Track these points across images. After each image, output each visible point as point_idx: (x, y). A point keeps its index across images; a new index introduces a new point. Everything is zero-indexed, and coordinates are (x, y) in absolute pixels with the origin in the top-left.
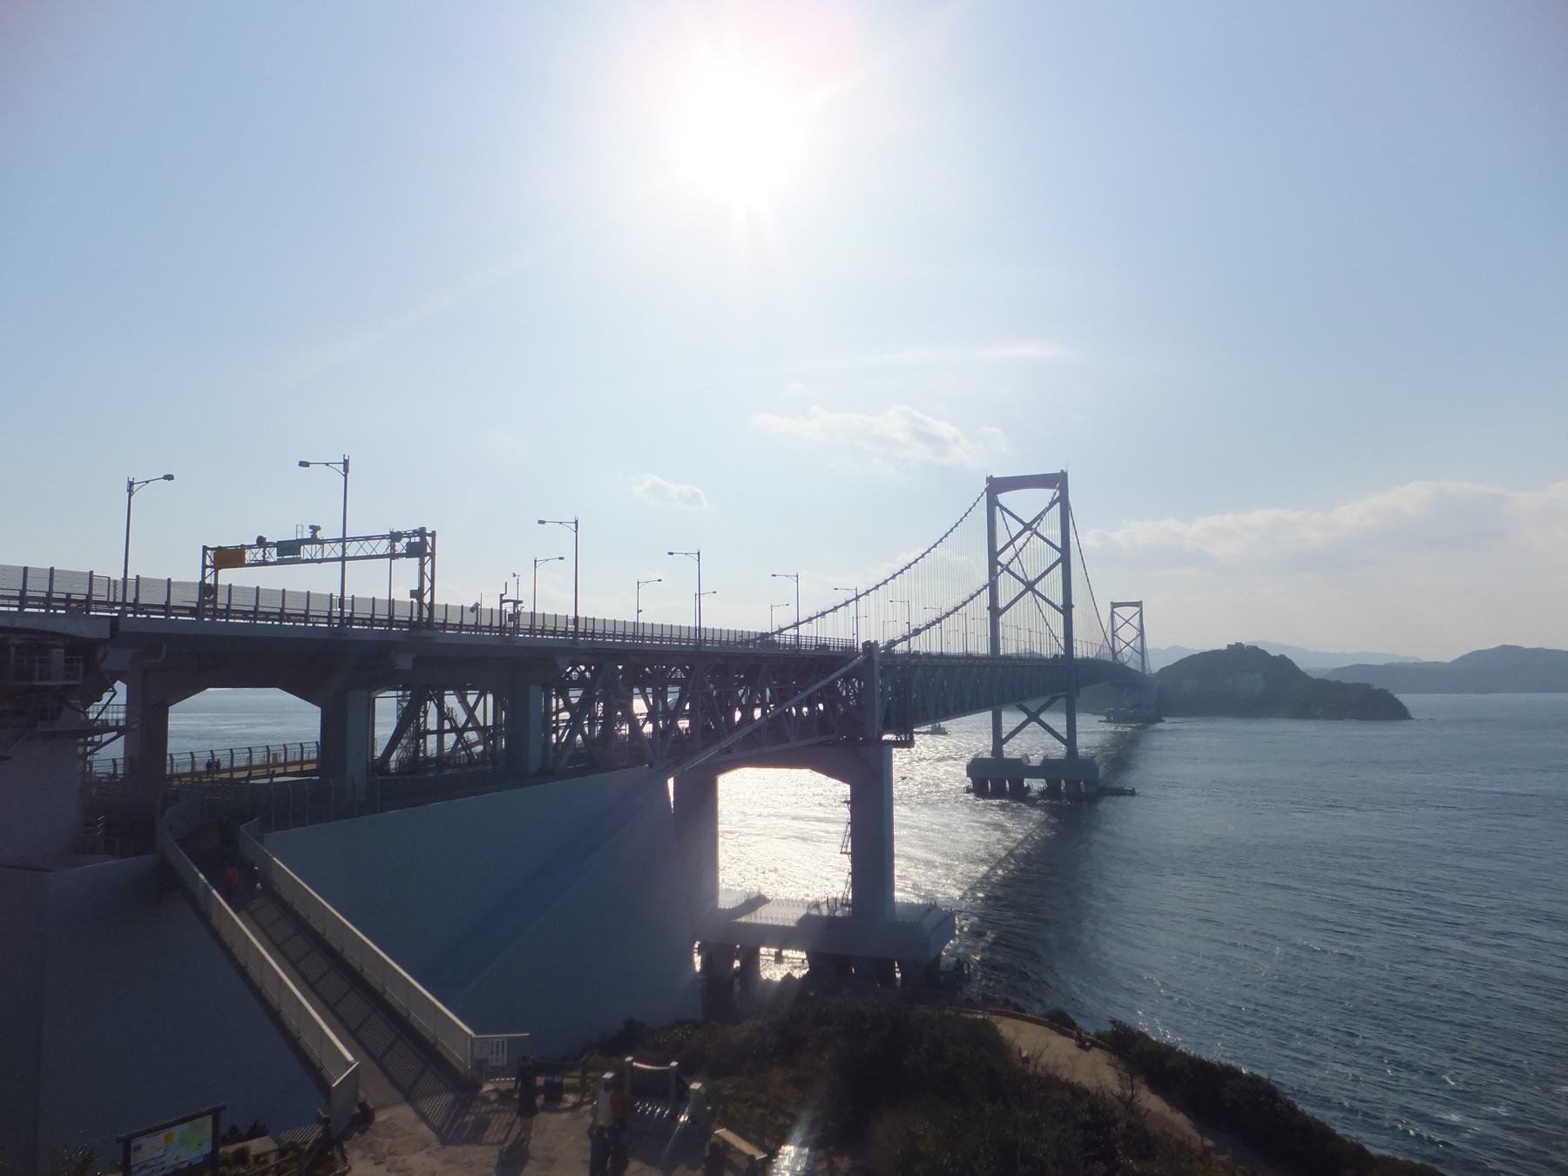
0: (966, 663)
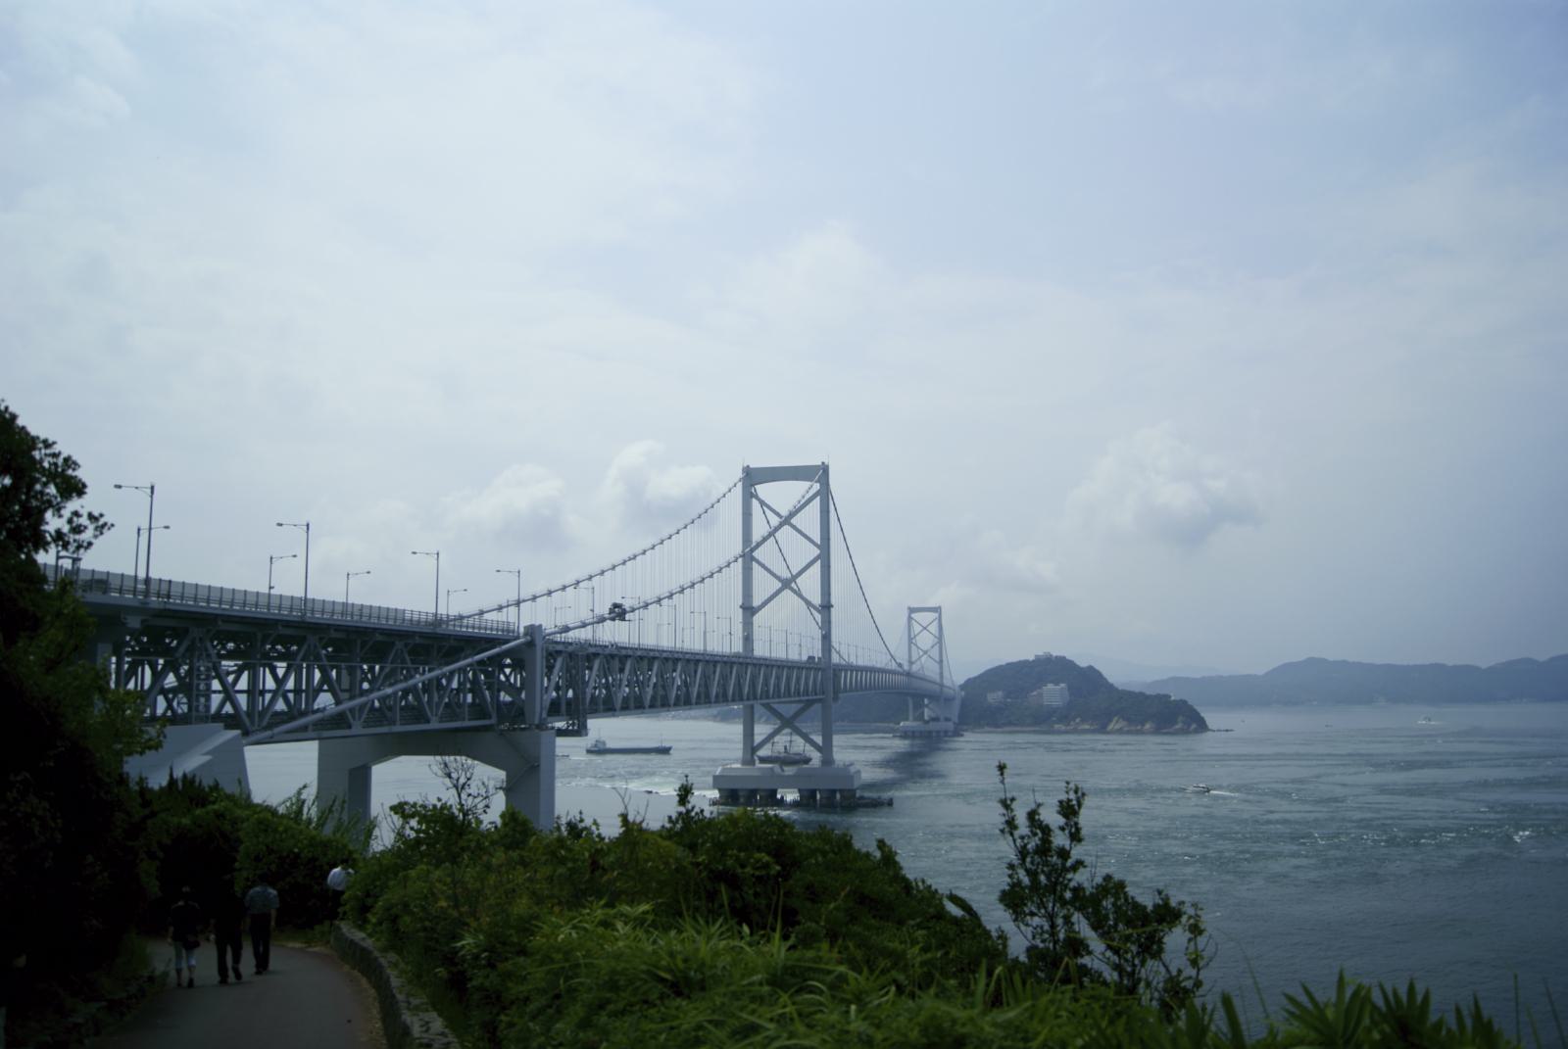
0: (727, 662)
